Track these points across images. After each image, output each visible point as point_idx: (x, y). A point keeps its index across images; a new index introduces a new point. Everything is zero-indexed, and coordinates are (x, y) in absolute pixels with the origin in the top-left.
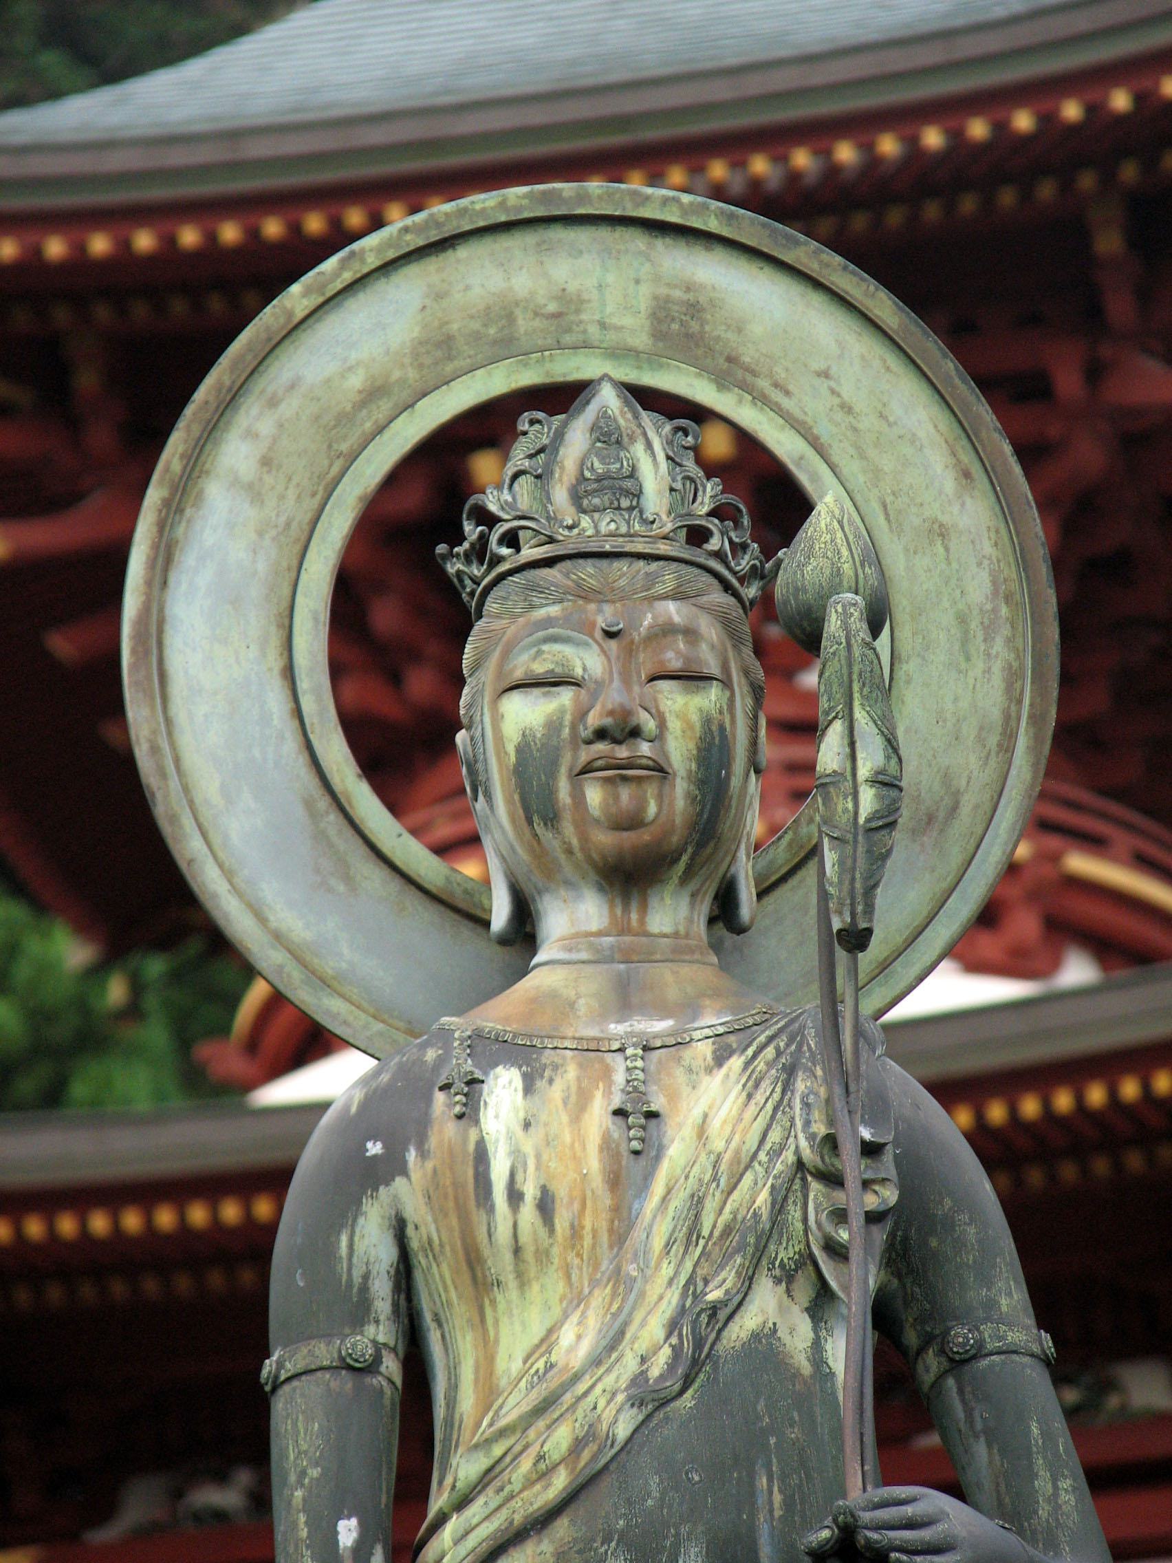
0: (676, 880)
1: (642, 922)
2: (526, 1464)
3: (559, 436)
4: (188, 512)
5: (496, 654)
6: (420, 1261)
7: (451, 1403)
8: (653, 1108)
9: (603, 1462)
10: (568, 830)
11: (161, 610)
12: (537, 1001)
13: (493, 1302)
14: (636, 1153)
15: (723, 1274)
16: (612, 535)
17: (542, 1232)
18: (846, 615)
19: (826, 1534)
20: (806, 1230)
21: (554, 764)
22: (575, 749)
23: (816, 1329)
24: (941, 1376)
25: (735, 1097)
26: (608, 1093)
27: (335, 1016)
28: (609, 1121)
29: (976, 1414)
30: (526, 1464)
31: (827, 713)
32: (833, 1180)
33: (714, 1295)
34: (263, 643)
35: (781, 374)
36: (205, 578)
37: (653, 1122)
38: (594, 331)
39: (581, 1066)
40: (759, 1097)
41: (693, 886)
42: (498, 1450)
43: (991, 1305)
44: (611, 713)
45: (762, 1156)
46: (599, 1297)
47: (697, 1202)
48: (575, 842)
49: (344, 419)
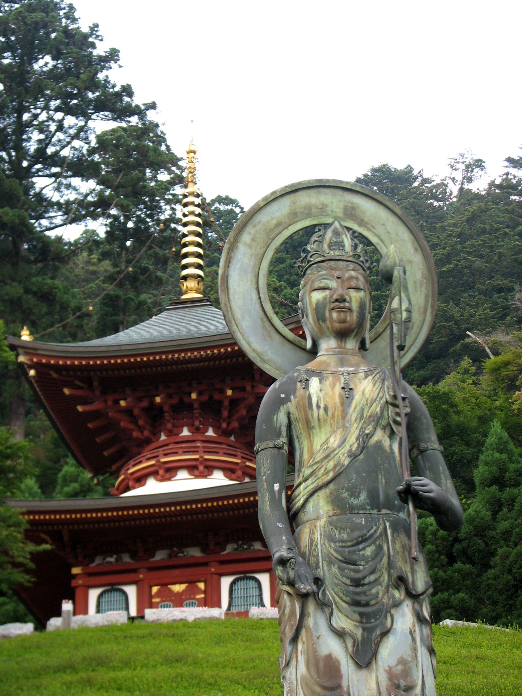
0: (353, 336)
1: (345, 346)
2: (322, 471)
3: (325, 233)
4: (234, 250)
5: (310, 283)
6: (294, 422)
7: (301, 456)
8: (351, 387)
9: (341, 470)
10: (328, 323)
11: (228, 273)
12: (321, 363)
13: (313, 432)
14: (347, 398)
15: (369, 427)
16: (338, 255)
17: (325, 415)
18: (399, 272)
19: (401, 487)
20: (389, 417)
21: (325, 307)
22: (330, 304)
23: (390, 441)
24: (417, 455)
25: (371, 385)
26: (340, 384)
27: (267, 369)
28: (341, 390)
29: (426, 464)
30: (322, 471)
31: (394, 294)
32: (395, 406)
33: (367, 432)
34: (252, 282)
35: (373, 225)
36: (238, 266)
37: (351, 391)
38: (330, 213)
39: (333, 377)
40: (377, 386)
41: (356, 338)
42: (315, 467)
43: (429, 438)
44: (339, 295)
45: (378, 399)
46: (339, 431)
47: (362, 410)
48: (330, 326)
49: (271, 230)
